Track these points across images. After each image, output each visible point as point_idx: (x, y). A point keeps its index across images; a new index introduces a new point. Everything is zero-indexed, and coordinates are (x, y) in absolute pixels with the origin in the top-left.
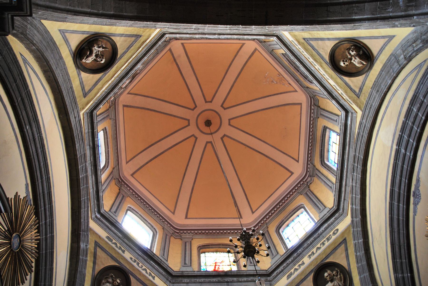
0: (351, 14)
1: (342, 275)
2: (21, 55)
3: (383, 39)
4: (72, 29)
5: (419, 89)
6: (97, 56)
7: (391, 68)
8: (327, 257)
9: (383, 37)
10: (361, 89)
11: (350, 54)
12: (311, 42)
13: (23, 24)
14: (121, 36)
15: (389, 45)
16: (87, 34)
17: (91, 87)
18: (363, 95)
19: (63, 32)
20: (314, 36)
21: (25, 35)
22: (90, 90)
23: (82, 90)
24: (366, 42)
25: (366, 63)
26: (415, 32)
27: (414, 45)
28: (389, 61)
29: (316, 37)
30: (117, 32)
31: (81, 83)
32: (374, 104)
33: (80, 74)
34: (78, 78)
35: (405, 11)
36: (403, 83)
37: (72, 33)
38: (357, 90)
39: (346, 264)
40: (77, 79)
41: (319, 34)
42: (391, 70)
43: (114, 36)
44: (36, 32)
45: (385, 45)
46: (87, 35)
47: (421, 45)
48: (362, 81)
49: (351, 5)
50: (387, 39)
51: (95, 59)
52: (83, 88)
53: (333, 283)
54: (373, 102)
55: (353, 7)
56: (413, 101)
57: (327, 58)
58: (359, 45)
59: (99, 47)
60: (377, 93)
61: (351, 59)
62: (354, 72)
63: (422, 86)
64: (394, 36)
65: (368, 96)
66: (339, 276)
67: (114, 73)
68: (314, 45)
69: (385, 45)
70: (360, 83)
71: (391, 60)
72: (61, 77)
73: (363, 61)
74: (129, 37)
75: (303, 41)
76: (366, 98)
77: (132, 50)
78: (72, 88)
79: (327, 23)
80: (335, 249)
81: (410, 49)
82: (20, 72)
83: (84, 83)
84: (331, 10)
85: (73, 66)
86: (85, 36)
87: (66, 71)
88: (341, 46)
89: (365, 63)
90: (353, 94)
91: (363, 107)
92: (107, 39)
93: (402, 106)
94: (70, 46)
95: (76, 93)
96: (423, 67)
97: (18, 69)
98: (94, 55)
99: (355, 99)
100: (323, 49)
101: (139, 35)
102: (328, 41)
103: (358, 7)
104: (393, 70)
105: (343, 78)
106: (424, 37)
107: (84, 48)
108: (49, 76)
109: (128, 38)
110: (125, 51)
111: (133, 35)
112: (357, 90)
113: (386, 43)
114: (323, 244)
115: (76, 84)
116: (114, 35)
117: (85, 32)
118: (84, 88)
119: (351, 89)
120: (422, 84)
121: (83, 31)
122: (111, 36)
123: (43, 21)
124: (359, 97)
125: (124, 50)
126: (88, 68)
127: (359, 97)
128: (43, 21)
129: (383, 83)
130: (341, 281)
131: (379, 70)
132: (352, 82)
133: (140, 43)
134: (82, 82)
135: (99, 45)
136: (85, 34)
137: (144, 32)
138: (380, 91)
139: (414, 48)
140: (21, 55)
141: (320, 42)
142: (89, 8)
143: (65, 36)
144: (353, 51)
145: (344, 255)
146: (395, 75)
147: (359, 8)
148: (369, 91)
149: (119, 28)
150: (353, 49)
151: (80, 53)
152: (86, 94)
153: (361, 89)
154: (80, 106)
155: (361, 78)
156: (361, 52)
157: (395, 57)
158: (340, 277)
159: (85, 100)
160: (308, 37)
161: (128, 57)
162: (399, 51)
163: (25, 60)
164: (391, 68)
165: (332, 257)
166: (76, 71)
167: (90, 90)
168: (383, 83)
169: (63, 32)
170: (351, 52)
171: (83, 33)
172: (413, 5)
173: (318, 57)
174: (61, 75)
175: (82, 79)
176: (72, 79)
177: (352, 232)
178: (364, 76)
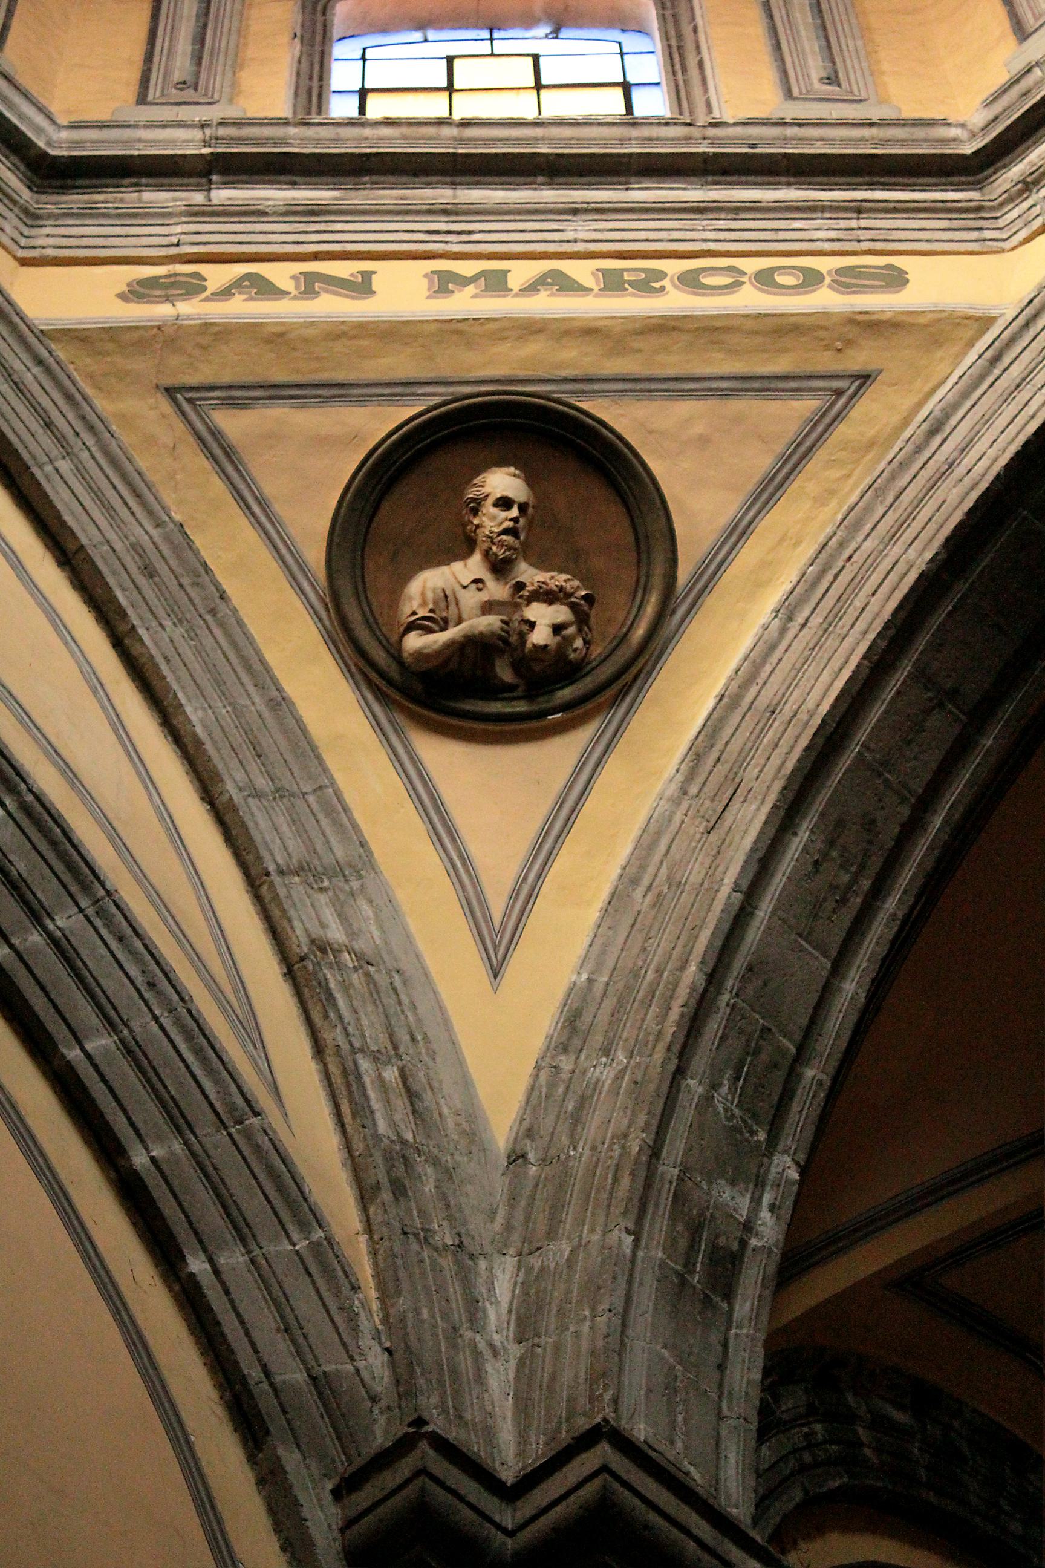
0: (833, 831)
3: (508, 886)
5: (120, 939)
7: (280, 792)
9: (526, 894)
10: (222, 455)
11: (549, 597)
12: (805, 407)
15: (445, 886)
18: (167, 439)
20: (831, 464)
24: (556, 756)
25: (420, 655)
26: (473, 1134)
27: (391, 1074)
28: (330, 812)
29: (813, 465)
32: (64, 466)
35: (679, 1198)
36: (157, 809)
38: (232, 423)
41: (821, 501)
42: (262, 782)
45: (460, 866)
47: (382, 1127)
48: (277, 507)
49: (876, 863)
50: (497, 907)
54: (80, 470)
55: (862, 867)
56: (54, 844)
57: (621, 417)
58: (566, 694)
60: (137, 548)
61: (500, 568)
62: (386, 506)
63: (134, 972)
65: (142, 463)
68: (773, 407)
69: (460, 866)
70: (272, 486)
71: (325, 822)
73: (450, 644)
75: (857, 360)
76: (126, 438)
79: (893, 641)
81: (376, 1039)
84: (934, 721)
88: (628, 577)
89: (414, 642)
90: (226, 378)
91: (78, 365)
93: (54, 754)
96: (243, 1046)
99: (174, 361)
100: (704, 441)
102: (723, 520)
103: (843, 902)
104: (258, 795)
105: (392, 399)
106: (429, 1187)
112: (232, 423)
113: (476, 881)
119: (275, 392)
120: (151, 985)
124: (170, 392)
127: (170, 392)
129: (189, 655)
131: (291, 689)
132: (323, 442)
138: (142, 581)
139: (376, 1059)
141: (762, 462)
144: (557, 629)
146: (231, 789)
147: (830, 905)
148: (169, 498)
150: (568, 640)
153: (222, 455)
155: (311, 523)
156: (505, 673)
157: (339, 871)
160: (858, 411)
162: (371, 937)
164: (280, 792)
168: (189, 655)
169: (497, 949)
170: (561, 613)
172: (692, 1272)
173: (673, 362)
178: (315, 554)
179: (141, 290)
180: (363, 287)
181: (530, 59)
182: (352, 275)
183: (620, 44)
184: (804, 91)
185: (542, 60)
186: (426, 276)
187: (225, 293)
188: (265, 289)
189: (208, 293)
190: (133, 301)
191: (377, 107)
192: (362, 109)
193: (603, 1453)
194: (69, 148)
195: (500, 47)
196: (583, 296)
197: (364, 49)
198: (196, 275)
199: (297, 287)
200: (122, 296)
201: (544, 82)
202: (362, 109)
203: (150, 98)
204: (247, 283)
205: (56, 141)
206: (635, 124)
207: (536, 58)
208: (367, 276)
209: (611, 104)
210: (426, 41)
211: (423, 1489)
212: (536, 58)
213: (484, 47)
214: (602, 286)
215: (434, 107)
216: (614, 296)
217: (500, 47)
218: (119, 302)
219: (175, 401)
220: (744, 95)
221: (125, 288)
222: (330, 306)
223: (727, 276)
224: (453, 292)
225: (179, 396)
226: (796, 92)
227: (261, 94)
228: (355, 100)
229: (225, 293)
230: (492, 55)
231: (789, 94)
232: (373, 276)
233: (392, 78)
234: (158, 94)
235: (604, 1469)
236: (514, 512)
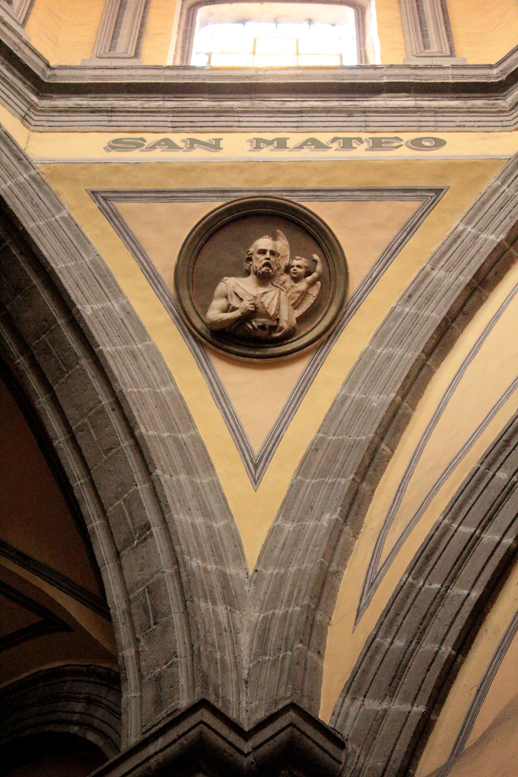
1: (315, 292)
8: (317, 193)
39: (365, 272)
53: (261, 290)
64: (256, 481)
66: (302, 286)
80: (376, 192)
114: (347, 144)
130: (296, 306)
145: (385, 237)
155: (166, 258)
158: (304, 294)
165: (338, 206)
169: (257, 467)
177: (484, 187)
179: (115, 145)
180: (216, 146)
182: (210, 140)
184: (418, 52)
186: (248, 141)
187: (301, 147)
188: (171, 145)
189: (144, 148)
193: (292, 715)
194: (333, 79)
196: (324, 151)
198: (142, 139)
199: (186, 146)
204: (309, 143)
206: (188, 68)
208: (218, 141)
214: (371, 145)
219: (97, 198)
221: (106, 145)
222: (199, 154)
224: (195, 148)
225: (98, 195)
227: (160, 54)
229: (153, 147)
233: (224, 45)
234: (102, 53)
235: (291, 725)
236: (268, 255)
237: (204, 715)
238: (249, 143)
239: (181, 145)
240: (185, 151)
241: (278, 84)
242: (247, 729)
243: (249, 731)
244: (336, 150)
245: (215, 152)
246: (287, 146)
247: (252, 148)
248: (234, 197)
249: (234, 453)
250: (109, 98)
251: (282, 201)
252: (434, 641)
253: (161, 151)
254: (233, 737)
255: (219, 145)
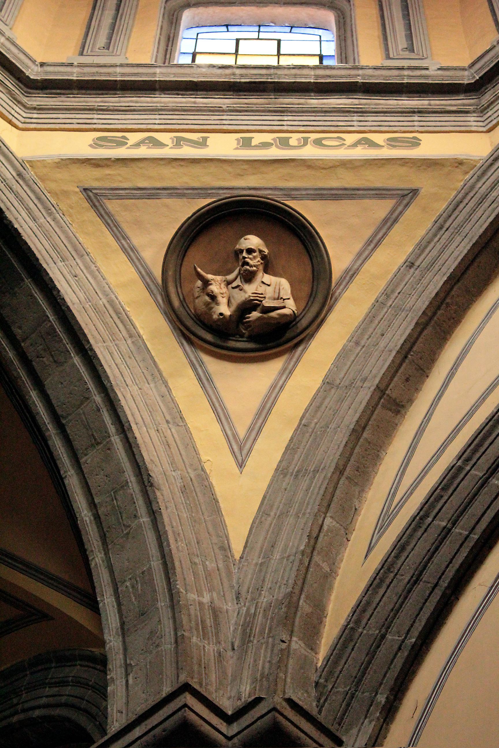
2: (370, 549)
4: (217, 428)
6: (249, 277)
13: (262, 632)
14: (133, 249)
16: (202, 363)
17: (366, 202)
19: (241, 449)
21: (291, 603)
22: (380, 193)
23: (396, 221)
30: (129, 273)
31: (374, 243)
33: (347, 271)
34: (366, 266)
37: (227, 417)
40: (373, 270)
43: (149, 274)
44: (277, 556)
45: (221, 414)
46: (207, 359)
51: (266, 271)
52: (390, 222)
59: (213, 297)
67: (264, 169)
69: (221, 414)
72: (388, 336)
74: (117, 225)
77: (150, 178)
78: (410, 264)
82: (415, 530)
83: (368, 233)
85: (333, 318)
86: (212, 364)
87: (365, 330)
92: (172, 290)
94: (273, 387)
95: (421, 232)
97: (407, 543)
98: (250, 290)
101: (89, 199)
107: (251, 339)
108: (407, 380)
109: (125, 227)
110: (170, 196)
111: (101, 216)
115: (389, 258)
116: (145, 274)
117: (200, 379)
118: (385, 221)
121: (203, 387)
122: (156, 284)
123: (237, 547)
125: (170, 201)
126: (309, 268)
128: (237, 547)
133: (107, 171)
134: (369, 242)
135: (207, 304)
136: (206, 372)
137: (66, 193)
140: (370, 549)
142: (109, 448)
143: (251, 429)
149: (112, 280)
151: (270, 337)
152: (404, 196)
154: (460, 180)
155: (154, 255)
159: (425, 183)
161: (182, 170)
163: (382, 526)
166: (347, 294)
167: (380, 193)
169: (241, 451)
171: (205, 381)
174: (382, 344)
175: (359, 254)
176: (382, 284)
180: (203, 144)
181: (276, 42)
182: (198, 138)
183: (320, 36)
184: (395, 54)
185: (282, 42)
186: (297, 139)
187: (137, 145)
188: (159, 144)
189: (128, 145)
190: (97, 148)
191: (200, 60)
192: (193, 60)
195: (262, 36)
197: (198, 34)
199: (173, 142)
200: (91, 146)
201: (282, 53)
202: (193, 60)
203: (85, 53)
204: (147, 141)
205: (33, 73)
207: (279, 41)
208: (205, 139)
209: (315, 61)
210: (228, 31)
211: (275, 718)
212: (279, 41)
213: (255, 35)
215: (229, 61)
216: (158, 148)
217: (262, 36)
218: (89, 147)
220: (370, 58)
223: (338, 141)
226: (391, 56)
227: (137, 51)
228: (190, 58)
230: (258, 39)
231: (388, 57)
232: (208, 139)
237: (189, 699)
238: (236, 141)
239: (382, 143)
240: (171, 148)
241: (218, 81)
242: (230, 713)
243: (232, 715)
244: (171, 148)
245: (201, 148)
246: (207, 144)
247: (239, 146)
248: (229, 194)
249: (219, 445)
250: (35, 94)
251: (227, 200)
252: (399, 633)
253: (147, 148)
254: (215, 720)
255: (206, 143)
